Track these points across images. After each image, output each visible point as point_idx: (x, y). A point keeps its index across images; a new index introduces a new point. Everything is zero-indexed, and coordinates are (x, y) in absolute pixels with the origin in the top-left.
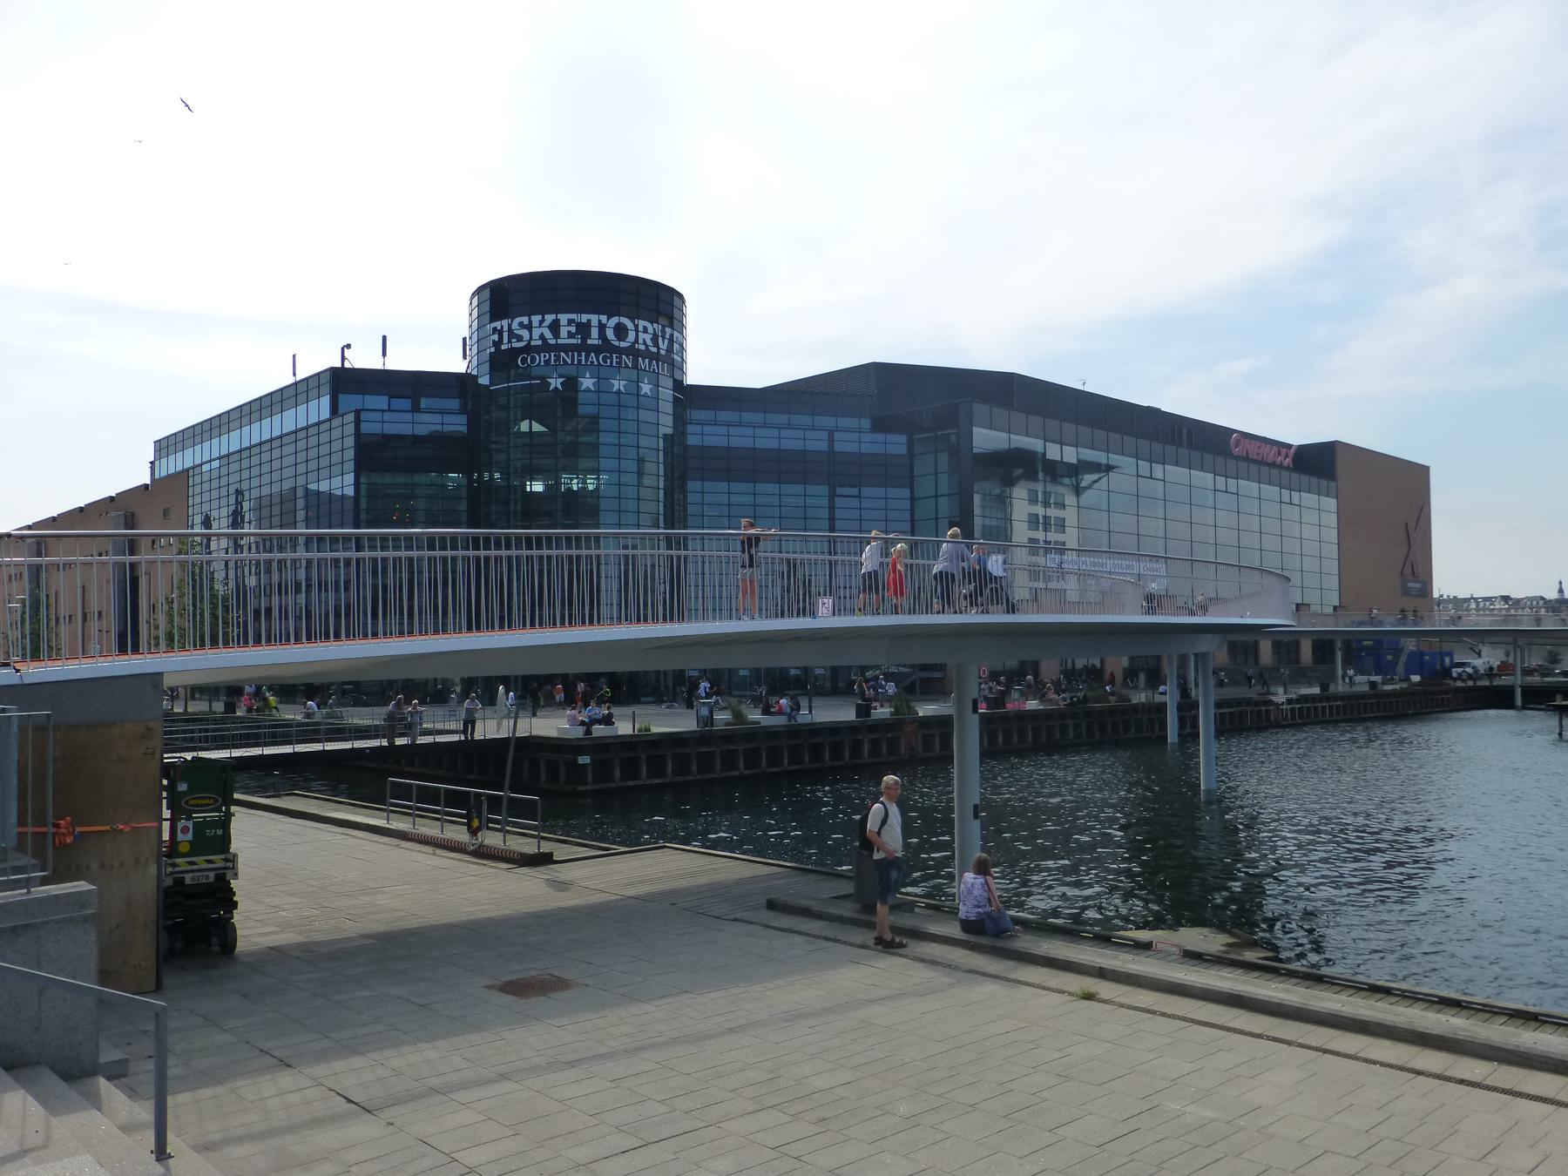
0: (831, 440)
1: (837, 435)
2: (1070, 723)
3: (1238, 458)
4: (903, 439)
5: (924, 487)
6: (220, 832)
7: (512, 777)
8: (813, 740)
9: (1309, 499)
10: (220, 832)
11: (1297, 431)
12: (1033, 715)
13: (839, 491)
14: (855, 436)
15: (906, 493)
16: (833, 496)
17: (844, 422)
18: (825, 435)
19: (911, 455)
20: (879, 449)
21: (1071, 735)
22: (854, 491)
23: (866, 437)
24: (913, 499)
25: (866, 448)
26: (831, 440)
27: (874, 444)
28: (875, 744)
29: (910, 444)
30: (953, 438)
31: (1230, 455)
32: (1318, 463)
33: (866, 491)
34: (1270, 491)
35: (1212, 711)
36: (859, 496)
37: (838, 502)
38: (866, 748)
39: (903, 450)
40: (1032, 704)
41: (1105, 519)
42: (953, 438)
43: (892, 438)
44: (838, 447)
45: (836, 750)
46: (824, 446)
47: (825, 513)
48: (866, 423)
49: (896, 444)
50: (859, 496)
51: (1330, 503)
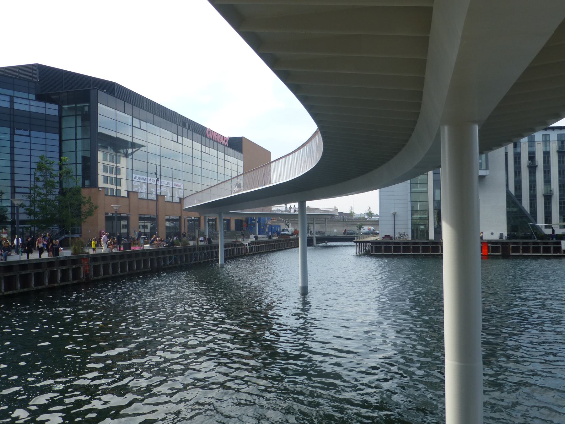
0: (12, 102)
1: (15, 100)
2: (119, 262)
3: (210, 139)
4: (56, 107)
5: (68, 134)
6: (413, 190)
7: (438, 298)
8: (23, 273)
9: (234, 160)
10: (413, 190)
11: (229, 133)
12: (150, 252)
13: (17, 132)
14: (27, 102)
15: (57, 137)
16: (12, 134)
17: (17, 94)
18: (8, 98)
19: (60, 117)
20: (42, 111)
21: (168, 263)
22: (27, 133)
23: (33, 103)
24: (61, 141)
25: (33, 109)
26: (12, 102)
27: (38, 107)
28: (64, 272)
29: (60, 110)
30: (86, 109)
31: (206, 137)
32: (236, 144)
33: (33, 133)
34: (221, 155)
35: (223, 249)
36: (30, 136)
37: (16, 138)
38: (59, 275)
39: (56, 113)
40: (147, 247)
41: (158, 160)
42: (86, 109)
43: (49, 105)
44: (16, 106)
45: (39, 278)
46: (7, 105)
47: (8, 144)
48: (33, 97)
49: (52, 109)
50: (30, 136)
51: (241, 163)
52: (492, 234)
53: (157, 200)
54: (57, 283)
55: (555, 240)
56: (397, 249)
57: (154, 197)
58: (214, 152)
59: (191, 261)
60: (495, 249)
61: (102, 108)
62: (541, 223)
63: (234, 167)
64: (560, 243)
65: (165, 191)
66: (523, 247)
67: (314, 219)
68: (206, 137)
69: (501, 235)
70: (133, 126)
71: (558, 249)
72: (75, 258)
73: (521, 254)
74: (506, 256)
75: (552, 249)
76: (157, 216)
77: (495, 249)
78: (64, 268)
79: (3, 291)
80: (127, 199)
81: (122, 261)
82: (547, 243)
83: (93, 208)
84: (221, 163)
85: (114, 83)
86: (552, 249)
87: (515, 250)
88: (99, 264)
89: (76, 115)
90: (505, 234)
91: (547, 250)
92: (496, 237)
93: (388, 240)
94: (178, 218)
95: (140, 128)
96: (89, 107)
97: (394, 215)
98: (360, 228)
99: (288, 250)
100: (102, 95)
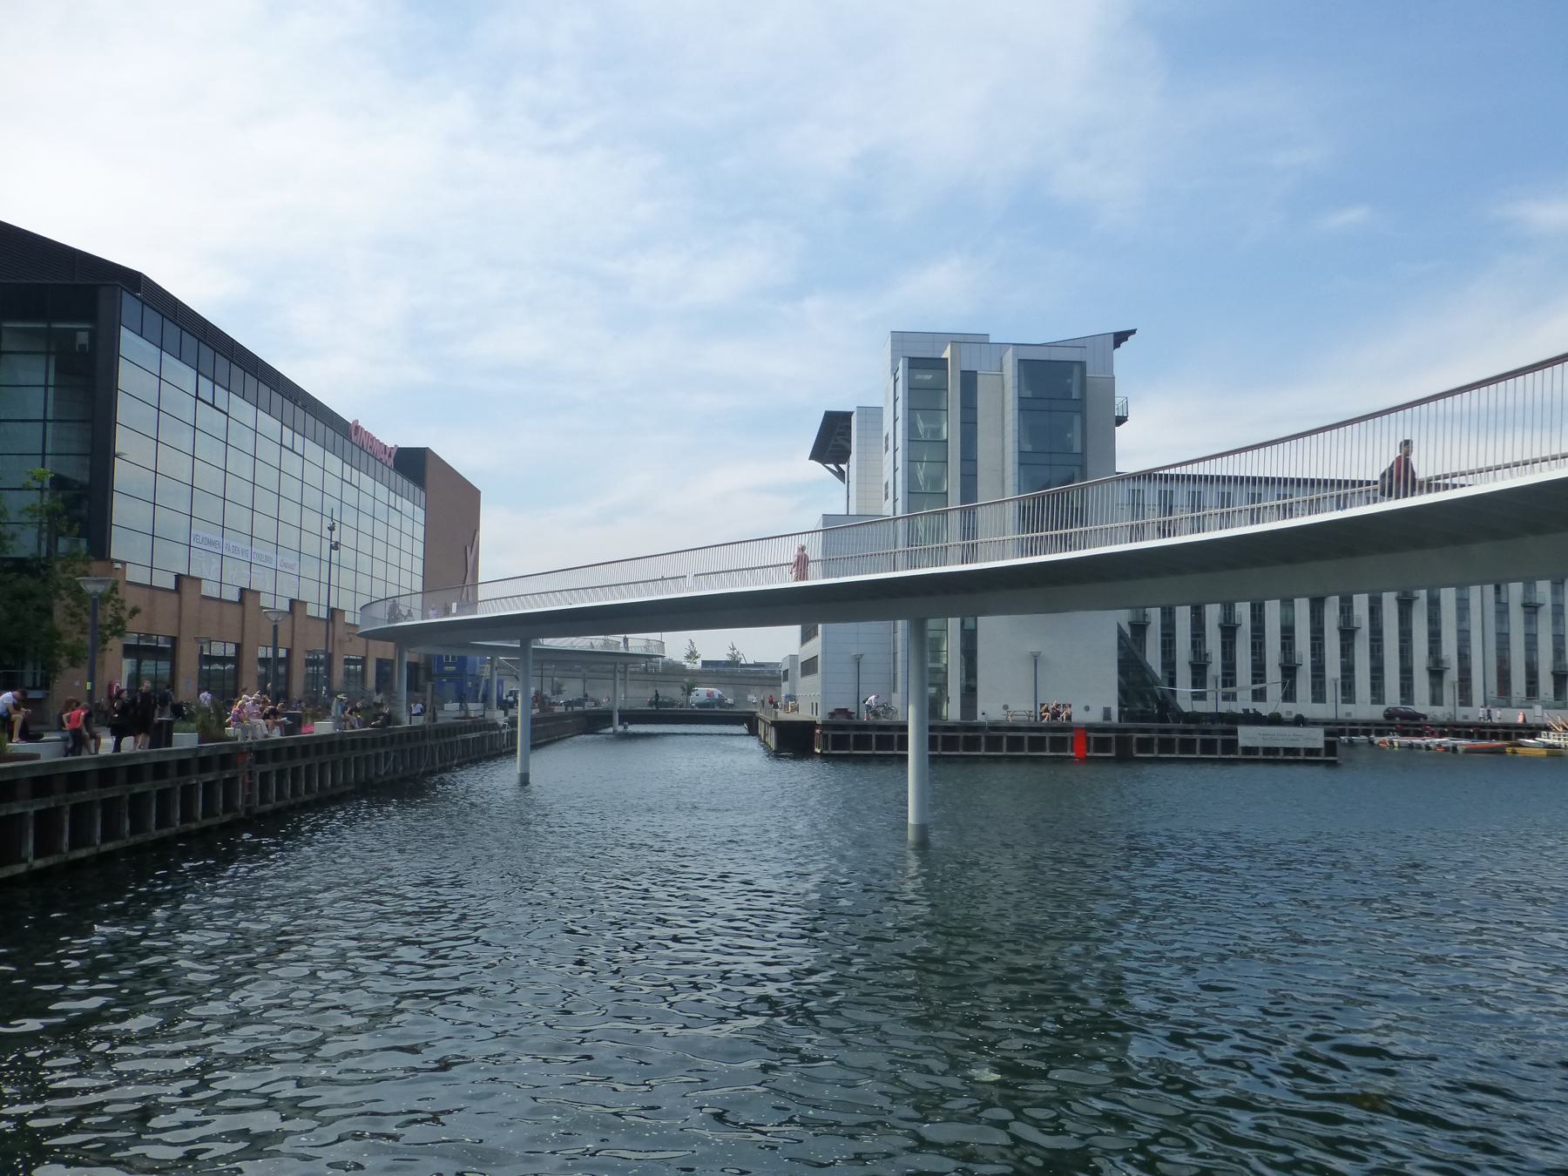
9: (407, 506)
11: (395, 435)
30: (83, 338)
31: (350, 439)
32: (414, 466)
42: (83, 338)
51: (420, 515)
52: (1087, 708)
53: (241, 601)
54: (195, 820)
55: (1225, 726)
56: (862, 742)
57: (233, 595)
58: (367, 482)
59: (309, 768)
60: (1102, 745)
61: (129, 342)
62: (1184, 688)
64: (1235, 732)
65: (261, 582)
66: (1161, 740)
67: (626, 665)
68: (350, 439)
69: (1107, 713)
70: (197, 397)
71: (1231, 745)
72: (227, 751)
73: (1004, 753)
74: (1124, 758)
75: (1219, 744)
76: (174, 641)
77: (1102, 745)
78: (137, 789)
79: (65, 848)
80: (175, 596)
81: (40, 805)
82: (1208, 732)
83: (125, 615)
85: (140, 274)
86: (1219, 744)
87: (1145, 745)
88: (117, 794)
89: (48, 353)
90: (1115, 710)
91: (1208, 746)
92: (1095, 717)
93: (843, 720)
94: (230, 650)
95: (213, 406)
96: (93, 335)
97: (858, 660)
98: (689, 690)
99: (557, 745)
100: (130, 305)
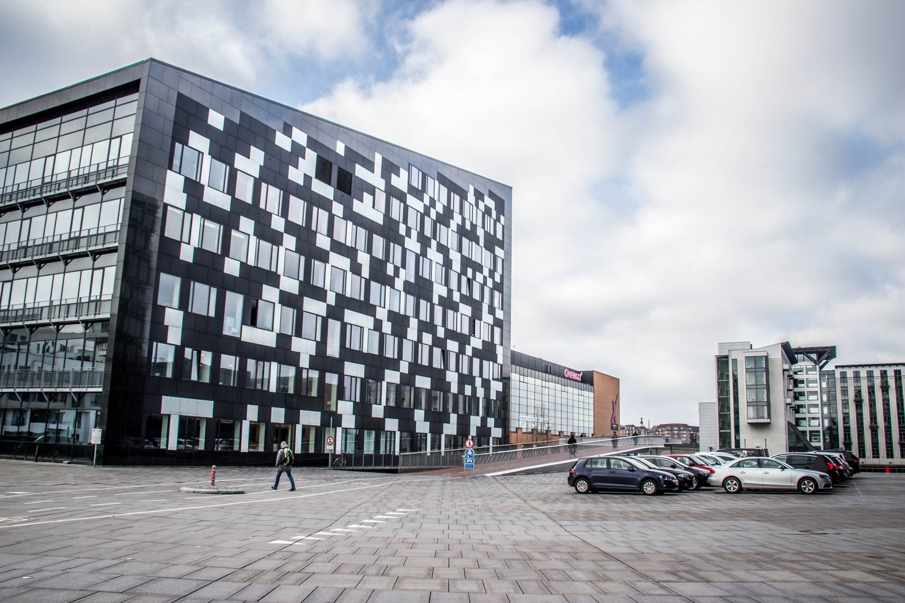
9: (586, 393)
32: (587, 379)
51: (591, 394)
63: (586, 400)
84: (576, 397)
